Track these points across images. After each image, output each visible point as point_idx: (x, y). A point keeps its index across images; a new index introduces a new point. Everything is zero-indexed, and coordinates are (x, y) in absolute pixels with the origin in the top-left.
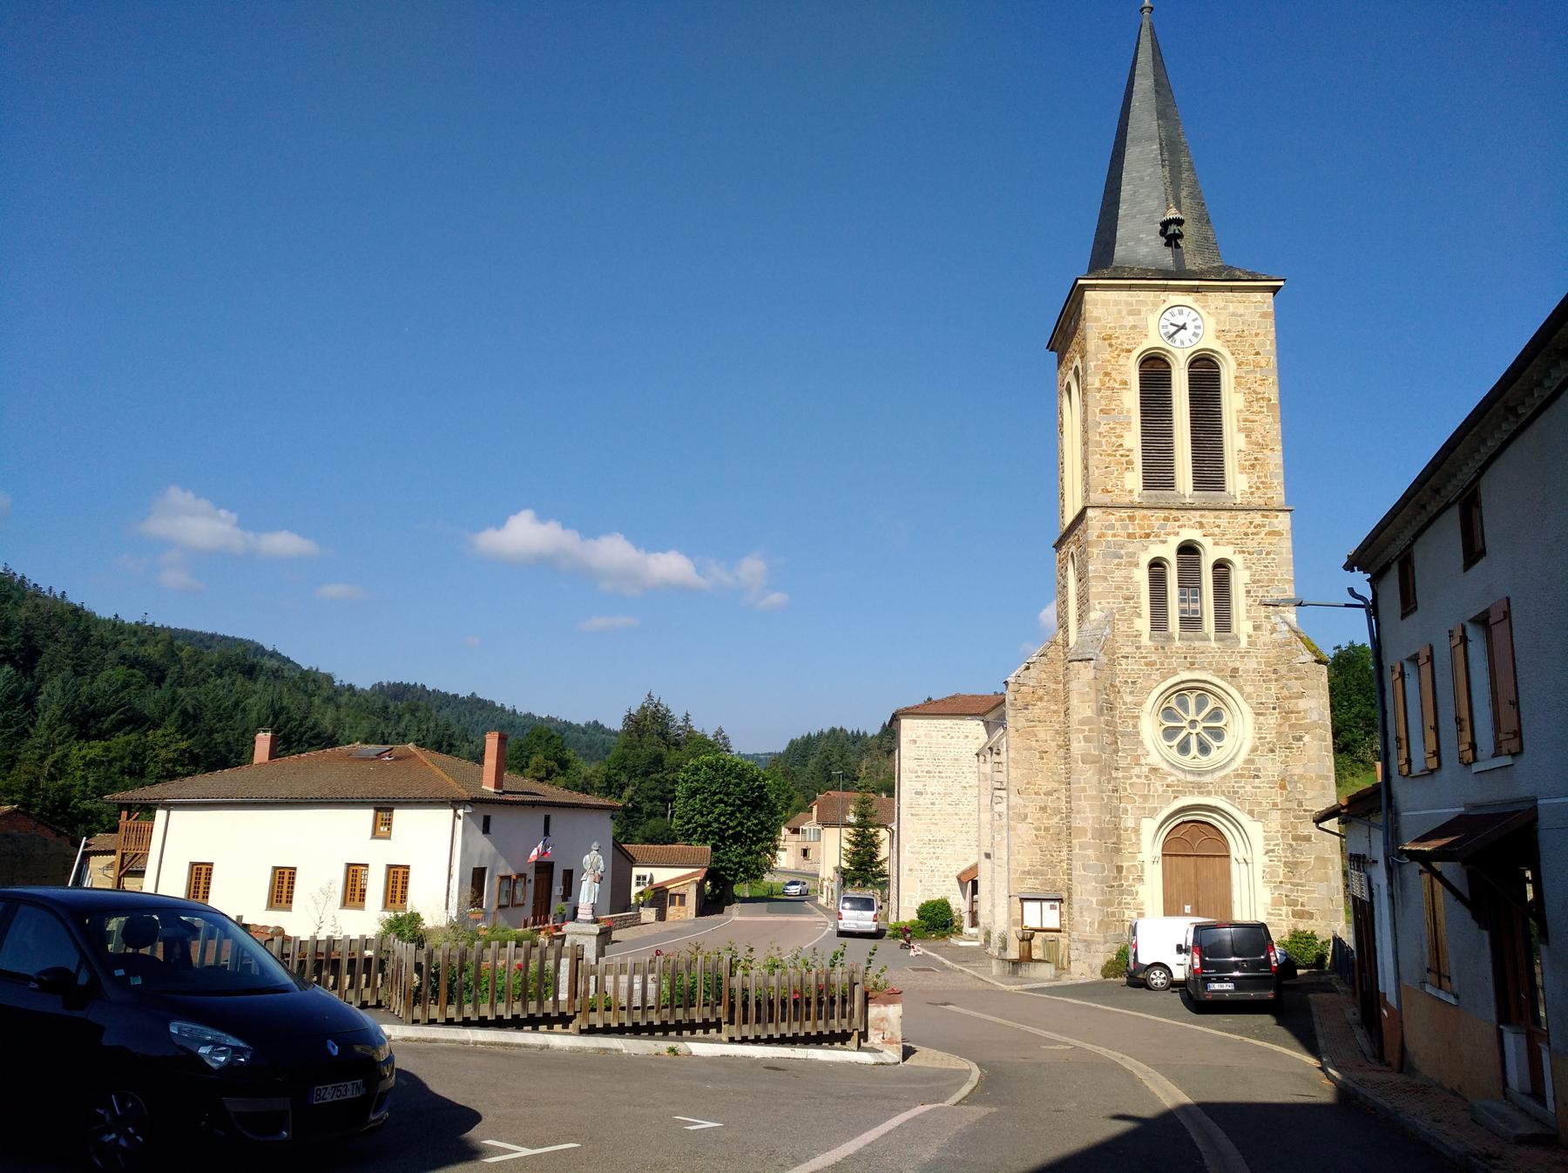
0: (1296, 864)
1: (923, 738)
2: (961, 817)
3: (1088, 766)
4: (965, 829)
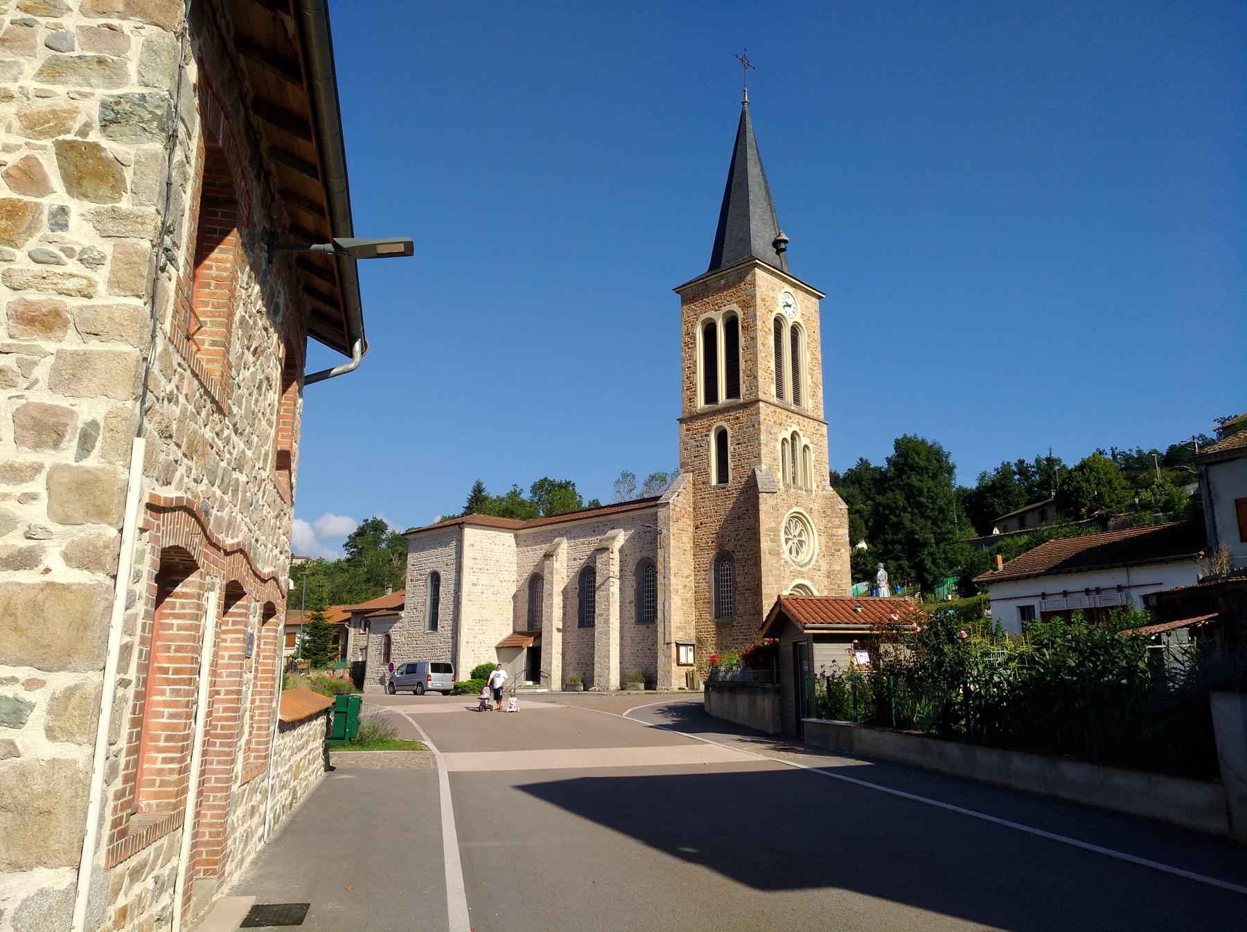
4: (501, 612)
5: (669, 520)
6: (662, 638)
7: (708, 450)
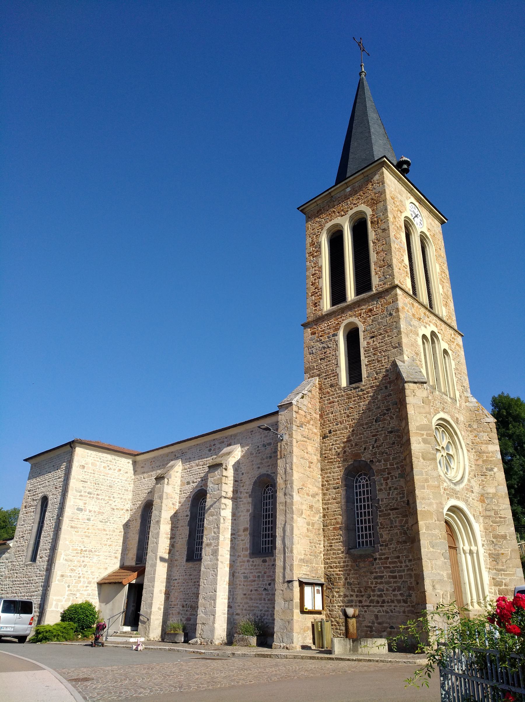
0: (498, 555)
1: (90, 465)
2: (108, 533)
3: (428, 462)
5: (291, 423)
6: (281, 575)
7: (337, 349)
